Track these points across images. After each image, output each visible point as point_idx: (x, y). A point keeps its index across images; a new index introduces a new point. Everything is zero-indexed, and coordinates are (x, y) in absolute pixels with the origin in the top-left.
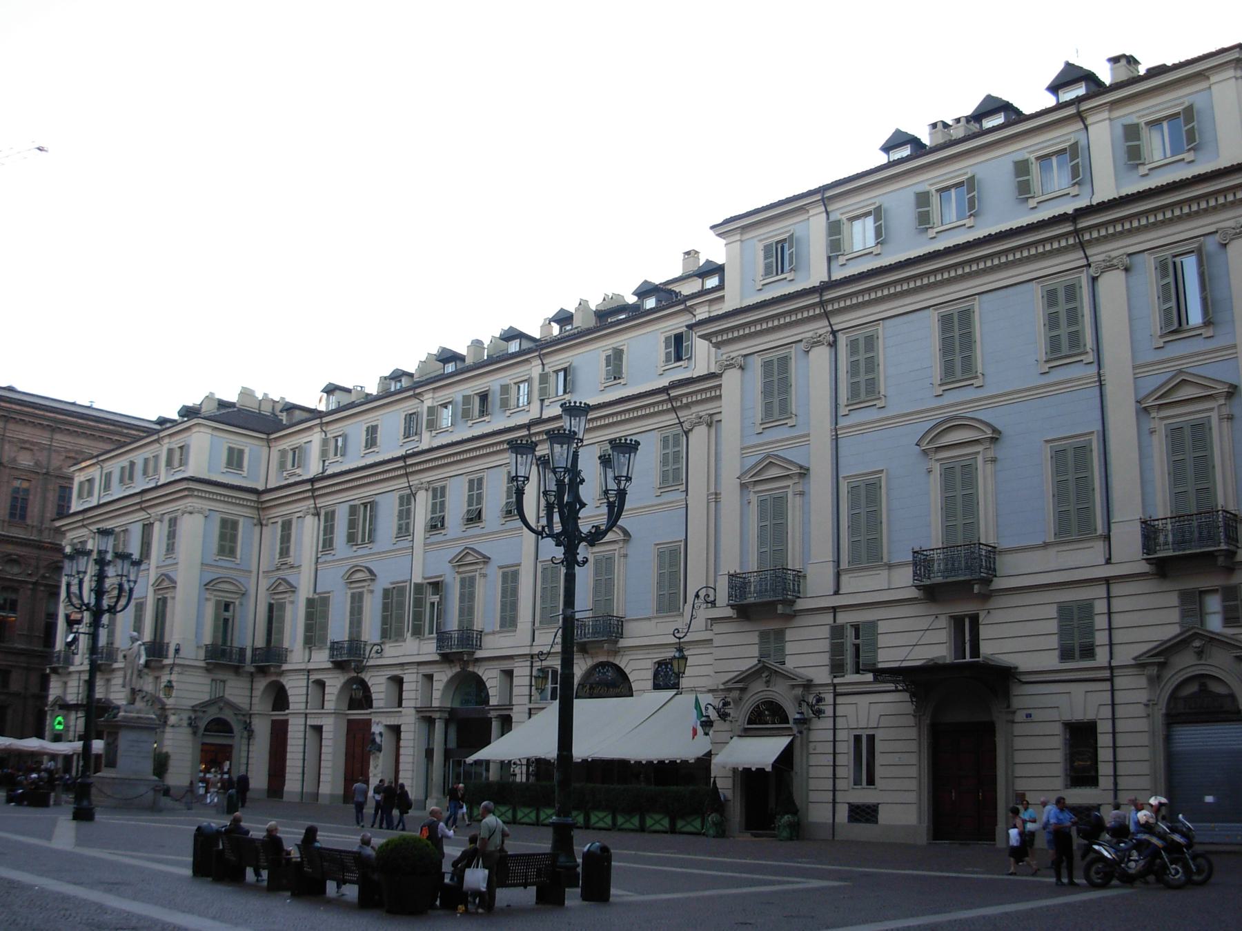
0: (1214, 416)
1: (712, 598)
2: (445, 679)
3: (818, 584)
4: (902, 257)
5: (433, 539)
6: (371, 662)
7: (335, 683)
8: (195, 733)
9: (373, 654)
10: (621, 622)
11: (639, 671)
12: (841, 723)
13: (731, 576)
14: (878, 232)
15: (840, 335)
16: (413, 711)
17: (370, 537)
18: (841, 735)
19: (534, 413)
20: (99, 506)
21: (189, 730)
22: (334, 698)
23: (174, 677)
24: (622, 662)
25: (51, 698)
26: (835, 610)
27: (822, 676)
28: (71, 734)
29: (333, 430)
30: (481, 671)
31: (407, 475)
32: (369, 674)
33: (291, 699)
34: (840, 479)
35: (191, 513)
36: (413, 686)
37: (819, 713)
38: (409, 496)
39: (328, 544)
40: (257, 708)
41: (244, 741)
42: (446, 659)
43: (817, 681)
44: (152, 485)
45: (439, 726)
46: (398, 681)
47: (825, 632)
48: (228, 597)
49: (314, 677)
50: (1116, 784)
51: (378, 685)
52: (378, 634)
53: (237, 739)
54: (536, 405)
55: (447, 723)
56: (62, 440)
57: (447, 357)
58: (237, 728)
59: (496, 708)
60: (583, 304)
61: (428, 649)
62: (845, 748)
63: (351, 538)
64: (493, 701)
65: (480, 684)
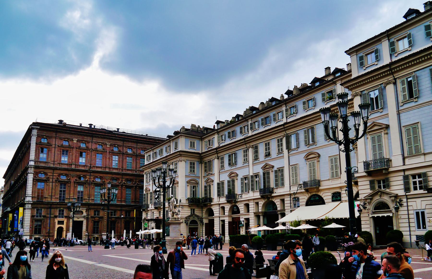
0: (383, 133)
1: (357, 170)
2: (262, 203)
3: (397, 163)
4: (422, 48)
5: (255, 162)
6: (239, 200)
7: (227, 207)
8: (187, 225)
9: (239, 198)
10: (319, 182)
11: (327, 196)
12: (410, 208)
13: (364, 162)
14: (410, 42)
15: (397, 80)
16: (253, 213)
17: (235, 163)
18: (410, 212)
19: (284, 121)
20: (153, 162)
21: (185, 224)
22: (228, 211)
23: (180, 209)
24: (321, 194)
25: (143, 218)
26: (404, 170)
27: (401, 193)
28: (150, 228)
29: (221, 134)
31: (246, 144)
32: (238, 204)
33: (214, 213)
34: (402, 127)
35: (181, 161)
36: (253, 206)
37: (401, 205)
38: (246, 150)
39: (222, 167)
40: (204, 216)
41: (201, 226)
42: (262, 197)
43: (399, 195)
44: (169, 154)
46: (247, 206)
47: (401, 178)
48: (194, 185)
49: (221, 206)
50: (409, 225)
51: (241, 207)
52: (240, 191)
53: (199, 226)
54: (285, 118)
56: (140, 145)
57: (252, 109)
58: (199, 222)
59: (280, 211)
60: (296, 87)
61: (257, 195)
62: (413, 216)
63: (230, 164)
64: (279, 209)
65: (274, 204)
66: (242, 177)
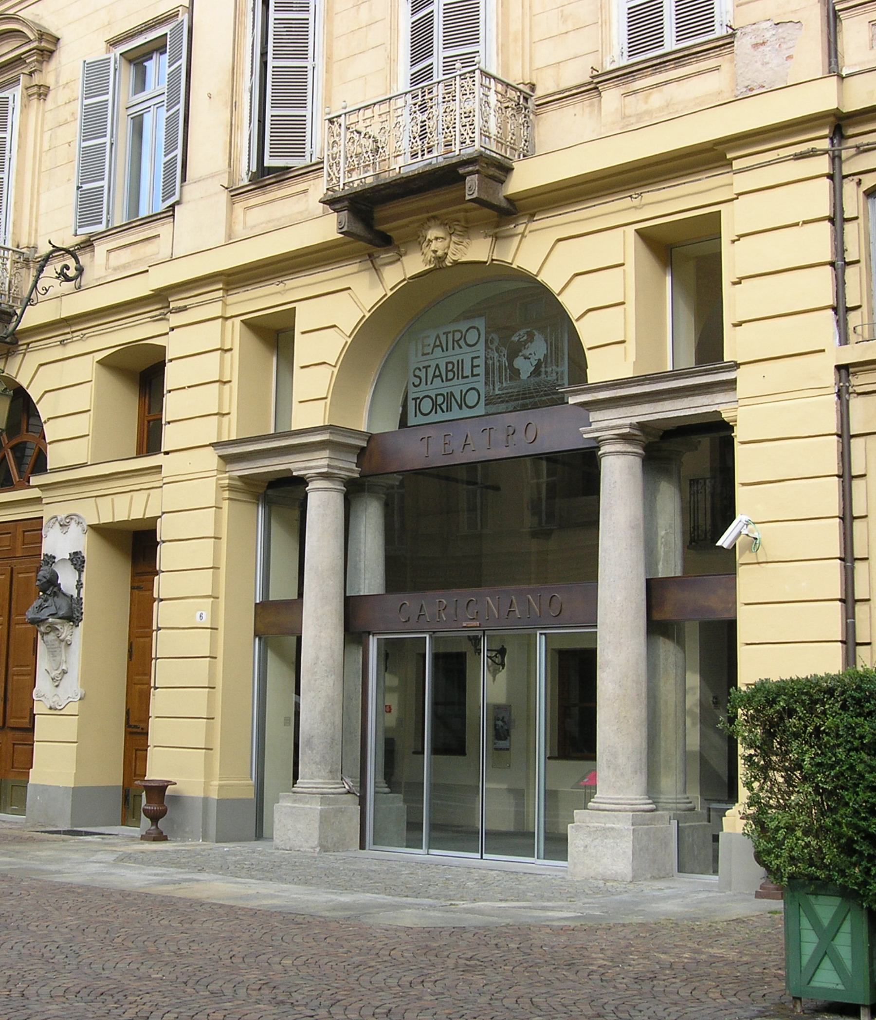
16: (210, 459)
30: (537, 252)
32: (33, 359)
45: (323, 506)
46: (143, 375)
55: (353, 492)
65: (531, 312)
66: (98, 51)
